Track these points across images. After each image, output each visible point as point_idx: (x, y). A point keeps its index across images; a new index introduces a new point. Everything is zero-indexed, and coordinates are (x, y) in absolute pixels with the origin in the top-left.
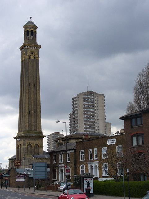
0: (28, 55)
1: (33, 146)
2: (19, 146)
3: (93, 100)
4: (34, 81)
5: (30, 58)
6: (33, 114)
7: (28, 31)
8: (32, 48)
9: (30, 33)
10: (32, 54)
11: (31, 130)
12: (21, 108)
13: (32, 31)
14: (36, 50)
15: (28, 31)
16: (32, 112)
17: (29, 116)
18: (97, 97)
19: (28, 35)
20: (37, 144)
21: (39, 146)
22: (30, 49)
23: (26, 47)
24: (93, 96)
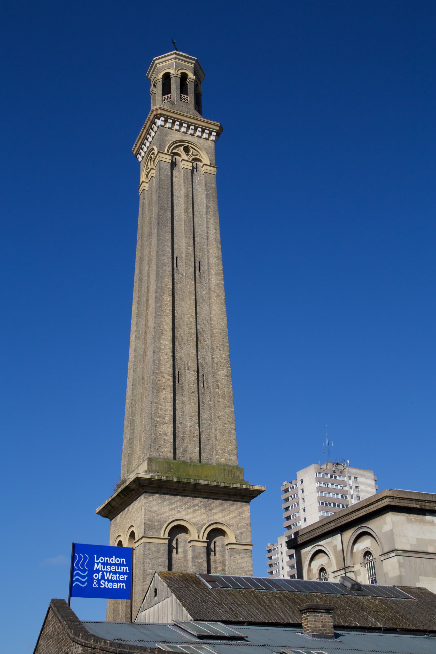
10: (187, 150)
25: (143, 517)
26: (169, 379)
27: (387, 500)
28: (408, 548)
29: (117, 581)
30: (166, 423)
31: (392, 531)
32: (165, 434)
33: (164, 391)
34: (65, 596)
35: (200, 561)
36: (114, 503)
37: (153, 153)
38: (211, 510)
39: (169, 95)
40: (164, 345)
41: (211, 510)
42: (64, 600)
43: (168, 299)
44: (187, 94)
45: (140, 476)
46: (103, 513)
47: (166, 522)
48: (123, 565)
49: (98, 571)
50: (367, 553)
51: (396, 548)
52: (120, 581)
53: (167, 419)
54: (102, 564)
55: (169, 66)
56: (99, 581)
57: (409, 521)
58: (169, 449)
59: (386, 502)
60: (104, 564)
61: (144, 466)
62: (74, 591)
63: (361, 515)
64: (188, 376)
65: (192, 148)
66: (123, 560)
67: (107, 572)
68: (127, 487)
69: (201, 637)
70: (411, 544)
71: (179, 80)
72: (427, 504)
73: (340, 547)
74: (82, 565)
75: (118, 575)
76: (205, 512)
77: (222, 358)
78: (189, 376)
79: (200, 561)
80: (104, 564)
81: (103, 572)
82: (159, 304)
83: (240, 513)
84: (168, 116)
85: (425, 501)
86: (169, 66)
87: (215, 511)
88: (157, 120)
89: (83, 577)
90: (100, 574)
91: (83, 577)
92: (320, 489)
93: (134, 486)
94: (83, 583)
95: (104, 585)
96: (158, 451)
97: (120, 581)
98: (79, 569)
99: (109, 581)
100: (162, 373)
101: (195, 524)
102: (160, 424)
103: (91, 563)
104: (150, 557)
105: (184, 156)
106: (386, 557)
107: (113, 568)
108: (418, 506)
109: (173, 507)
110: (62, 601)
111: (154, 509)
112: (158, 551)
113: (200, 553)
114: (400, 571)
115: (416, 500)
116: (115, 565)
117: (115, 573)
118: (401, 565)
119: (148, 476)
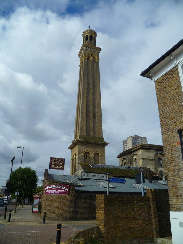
7: (87, 36)
19: (87, 39)
36: (167, 110)
42: (34, 173)
44: (92, 40)
50: (136, 159)
55: (88, 33)
57: (146, 151)
59: (140, 147)
61: (79, 138)
64: (90, 115)
69: (78, 179)
78: (91, 114)
85: (150, 147)
86: (88, 33)
92: (132, 142)
102: (83, 127)
105: (91, 57)
118: (143, 162)
119: (79, 140)
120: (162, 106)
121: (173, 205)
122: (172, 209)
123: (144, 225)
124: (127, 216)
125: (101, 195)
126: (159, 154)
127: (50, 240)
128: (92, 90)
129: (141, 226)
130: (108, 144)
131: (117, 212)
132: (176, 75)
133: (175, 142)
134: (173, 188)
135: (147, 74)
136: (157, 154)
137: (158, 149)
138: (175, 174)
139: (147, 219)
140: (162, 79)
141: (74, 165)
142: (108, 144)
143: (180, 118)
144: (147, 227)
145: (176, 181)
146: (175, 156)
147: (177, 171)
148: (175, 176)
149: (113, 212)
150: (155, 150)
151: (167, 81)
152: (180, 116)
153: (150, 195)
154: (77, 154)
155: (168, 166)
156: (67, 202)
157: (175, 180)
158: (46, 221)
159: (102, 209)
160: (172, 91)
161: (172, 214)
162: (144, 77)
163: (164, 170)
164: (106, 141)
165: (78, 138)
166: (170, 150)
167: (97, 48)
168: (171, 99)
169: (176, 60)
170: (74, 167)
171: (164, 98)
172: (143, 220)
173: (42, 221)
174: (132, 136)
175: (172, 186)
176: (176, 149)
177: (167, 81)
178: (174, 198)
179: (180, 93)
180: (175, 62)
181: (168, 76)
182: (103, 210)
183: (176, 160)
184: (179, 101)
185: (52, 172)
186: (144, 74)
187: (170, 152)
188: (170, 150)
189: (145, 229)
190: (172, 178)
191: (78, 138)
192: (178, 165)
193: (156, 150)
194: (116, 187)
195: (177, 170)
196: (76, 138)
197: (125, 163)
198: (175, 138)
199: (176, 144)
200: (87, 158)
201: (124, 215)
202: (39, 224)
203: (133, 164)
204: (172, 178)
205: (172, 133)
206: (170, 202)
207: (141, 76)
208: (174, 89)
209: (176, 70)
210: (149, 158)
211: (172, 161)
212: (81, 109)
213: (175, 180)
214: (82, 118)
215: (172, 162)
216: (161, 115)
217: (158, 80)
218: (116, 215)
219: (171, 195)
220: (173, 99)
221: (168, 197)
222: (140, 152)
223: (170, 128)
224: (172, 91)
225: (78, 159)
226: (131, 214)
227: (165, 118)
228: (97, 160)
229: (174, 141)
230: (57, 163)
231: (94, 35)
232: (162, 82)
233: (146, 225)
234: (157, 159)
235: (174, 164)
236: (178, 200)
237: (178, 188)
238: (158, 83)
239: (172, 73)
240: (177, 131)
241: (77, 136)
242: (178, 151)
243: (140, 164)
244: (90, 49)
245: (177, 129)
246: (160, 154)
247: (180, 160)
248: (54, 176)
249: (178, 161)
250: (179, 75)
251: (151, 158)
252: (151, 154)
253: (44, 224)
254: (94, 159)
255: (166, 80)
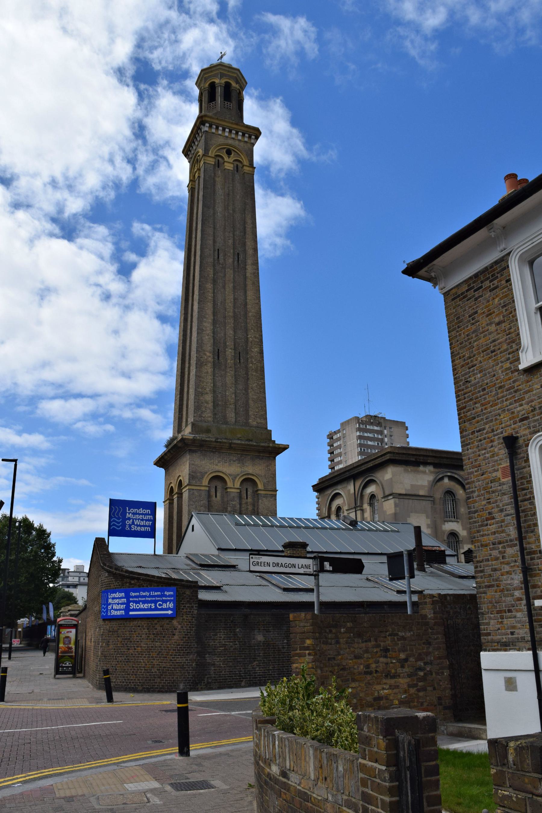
0: (212, 153)
1: (234, 486)
2: (176, 490)
3: (382, 444)
4: (234, 244)
5: (218, 165)
6: (230, 362)
7: (213, 86)
8: (227, 134)
9: (219, 91)
10: (229, 152)
11: (226, 423)
12: (185, 320)
13: (227, 86)
14: (242, 144)
15: (213, 86)
16: (230, 352)
17: (214, 366)
18: (390, 428)
19: (212, 97)
20: (249, 481)
21: (260, 486)
22: (223, 136)
23: (206, 128)
24: (379, 424)
25: (188, 469)
26: (210, 357)
27: (388, 455)
28: (403, 492)
29: (144, 526)
30: (207, 393)
31: (391, 479)
32: (207, 403)
33: (206, 367)
34: (105, 535)
35: (234, 503)
37: (199, 156)
38: (243, 464)
39: (214, 103)
40: (206, 328)
41: (243, 464)
43: (210, 287)
45: (184, 437)
46: (158, 465)
47: (206, 473)
48: (148, 514)
49: (129, 519)
50: (373, 497)
51: (394, 492)
52: (146, 526)
53: (208, 389)
54: (132, 514)
56: (130, 525)
57: (406, 471)
58: (209, 415)
59: (388, 457)
60: (134, 514)
62: (112, 532)
63: (377, 463)
65: (234, 150)
66: (148, 511)
67: (136, 519)
68: (175, 445)
70: (406, 489)
71: (223, 89)
72: (422, 458)
73: (352, 491)
74: (118, 514)
75: (144, 522)
76: (239, 465)
77: (255, 337)
79: (234, 503)
80: (134, 514)
81: (133, 519)
82: (202, 292)
83: (267, 466)
84: (212, 122)
85: (420, 455)
87: (247, 464)
88: (202, 126)
89: (119, 523)
90: (131, 521)
91: (119, 523)
93: (180, 445)
94: (118, 527)
95: (134, 528)
96: (201, 416)
97: (146, 526)
98: (115, 517)
99: (137, 526)
100: (204, 351)
101: (230, 475)
102: (202, 394)
103: (125, 513)
104: (193, 500)
106: (386, 499)
107: (141, 517)
108: (414, 460)
109: (212, 461)
110: (103, 539)
111: (196, 463)
112: (200, 496)
113: (234, 497)
114: (395, 510)
115: (413, 455)
116: (142, 514)
117: (142, 520)
118: (396, 505)
119: (191, 437)
120: (463, 366)
121: (489, 634)
122: (486, 646)
123: (412, 691)
124: (368, 666)
125: (303, 614)
126: (446, 480)
127: (156, 742)
128: (232, 272)
129: (405, 692)
130: (284, 448)
131: (342, 659)
132: (503, 282)
133: (496, 468)
134: (491, 593)
135: (422, 272)
136: (442, 479)
137: (444, 462)
138: (495, 553)
139: (422, 674)
140: (465, 288)
141: (175, 517)
142: (284, 448)
143: (511, 404)
144: (421, 694)
145: (499, 573)
146: (498, 506)
147: (500, 546)
148: (497, 559)
149: (334, 658)
150: (434, 467)
151: (479, 297)
152: (511, 398)
153: (428, 611)
154: (186, 481)
155: (478, 531)
156: (176, 637)
157: (495, 570)
158: (116, 695)
159: (307, 652)
160: (493, 328)
161: (487, 659)
162: (413, 277)
163: (461, 528)
164: (278, 438)
165: (187, 431)
166: (485, 489)
167: (248, 127)
168: (488, 349)
169: (505, 239)
170: (175, 525)
171: (470, 343)
172: (409, 676)
173: (103, 694)
174: (357, 418)
175: (489, 586)
176: (499, 488)
177: (479, 297)
178: (492, 616)
179: (513, 335)
180: (502, 246)
181: (482, 282)
182: (309, 654)
183: (499, 517)
184: (511, 356)
185: (118, 545)
186: (412, 270)
187: (482, 495)
188: (485, 489)
189: (416, 700)
190: (487, 566)
191: (187, 431)
192: (503, 532)
193: (436, 465)
194: (225, 588)
195: (500, 543)
196: (179, 428)
197: (339, 509)
198: (496, 458)
199: (499, 474)
200: (218, 494)
201: (362, 667)
202: (94, 706)
203: (363, 511)
204: (487, 566)
205: (490, 444)
206: (482, 627)
207: (406, 276)
208: (497, 320)
209: (505, 268)
210: (417, 493)
211: (487, 519)
212: (195, 334)
213: (495, 570)
214: (200, 364)
215: (489, 522)
216: (460, 391)
217: (454, 291)
218: (342, 667)
219: (484, 608)
220: (494, 351)
221: (477, 614)
222: (388, 474)
223: (484, 429)
224: (493, 328)
225: (190, 499)
226: (377, 662)
227: (471, 400)
228: (249, 500)
229: (493, 466)
230: (125, 517)
231: (237, 82)
232: (464, 297)
233: (419, 690)
234: (438, 495)
235: (493, 528)
236: (502, 623)
237: (502, 591)
238: (453, 300)
239: (492, 276)
240: (502, 441)
241: (184, 424)
242: (504, 494)
243: (388, 513)
244: (224, 130)
245: (505, 434)
246: (451, 478)
247: (509, 517)
248: (117, 556)
249: (503, 521)
250: (511, 285)
251: (421, 493)
252: (421, 479)
253: (110, 705)
254: (240, 498)
255: (477, 294)
